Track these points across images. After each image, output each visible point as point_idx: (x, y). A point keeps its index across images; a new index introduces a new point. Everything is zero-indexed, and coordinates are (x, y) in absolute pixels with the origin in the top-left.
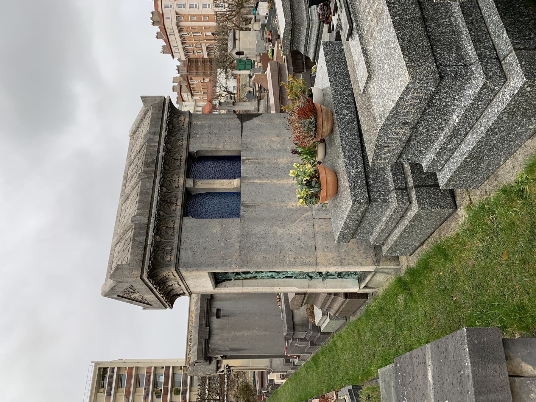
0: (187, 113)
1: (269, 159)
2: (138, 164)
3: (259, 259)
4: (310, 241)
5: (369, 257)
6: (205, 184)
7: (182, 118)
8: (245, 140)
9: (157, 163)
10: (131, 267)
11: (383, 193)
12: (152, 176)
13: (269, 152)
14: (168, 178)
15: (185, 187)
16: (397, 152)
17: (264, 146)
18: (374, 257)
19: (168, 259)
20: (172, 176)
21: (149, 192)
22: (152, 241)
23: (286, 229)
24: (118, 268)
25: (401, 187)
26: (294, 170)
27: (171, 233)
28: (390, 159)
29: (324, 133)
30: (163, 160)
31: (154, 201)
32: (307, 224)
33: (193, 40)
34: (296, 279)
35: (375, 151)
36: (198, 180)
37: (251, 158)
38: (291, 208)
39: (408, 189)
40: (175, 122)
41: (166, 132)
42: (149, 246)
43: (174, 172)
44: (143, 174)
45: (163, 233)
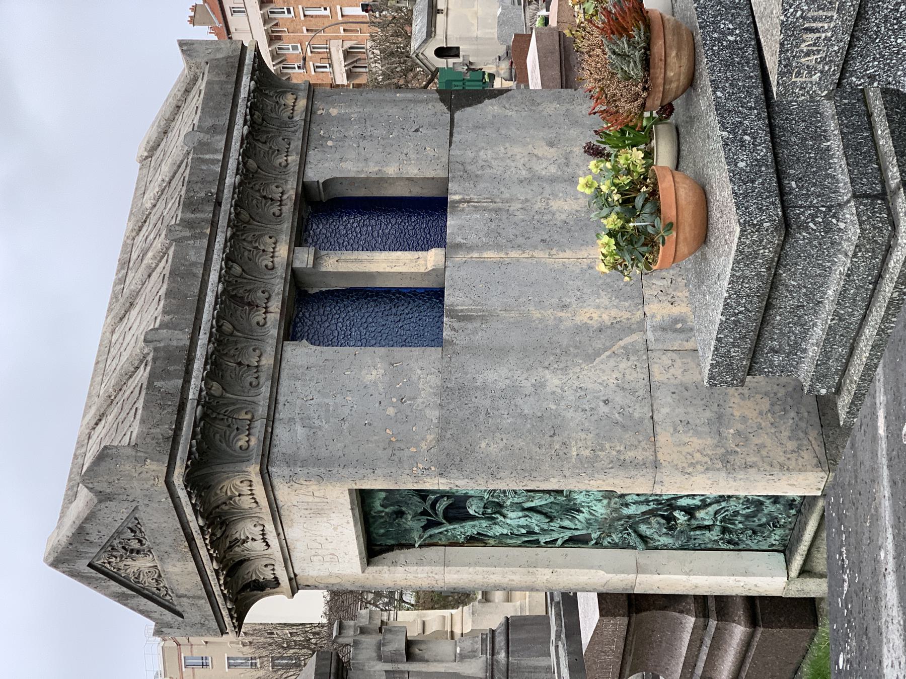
0: (303, 88)
1: (527, 200)
2: (165, 214)
3: (494, 449)
4: (637, 406)
5: (804, 448)
6: (346, 261)
7: (289, 99)
8: (459, 153)
9: (218, 203)
10: (139, 454)
11: (824, 209)
12: (205, 234)
13: (525, 183)
14: (245, 244)
15: (292, 268)
16: (836, 48)
17: (513, 169)
18: (820, 451)
19: (240, 443)
20: (257, 238)
21: (194, 270)
22: (201, 390)
23: (571, 375)
24: (103, 456)
25: (869, 192)
26: (590, 177)
27: (250, 379)
28: (821, 72)
29: (671, 82)
30: (236, 196)
31: (209, 293)
32: (630, 363)
33: (304, 29)
34: (602, 547)
35: (782, 44)
36: (326, 252)
37: (476, 197)
38: (586, 323)
39: (889, 197)
40: (269, 108)
41: (246, 127)
42: (192, 403)
43: (264, 230)
44: (180, 228)
45: (229, 378)
